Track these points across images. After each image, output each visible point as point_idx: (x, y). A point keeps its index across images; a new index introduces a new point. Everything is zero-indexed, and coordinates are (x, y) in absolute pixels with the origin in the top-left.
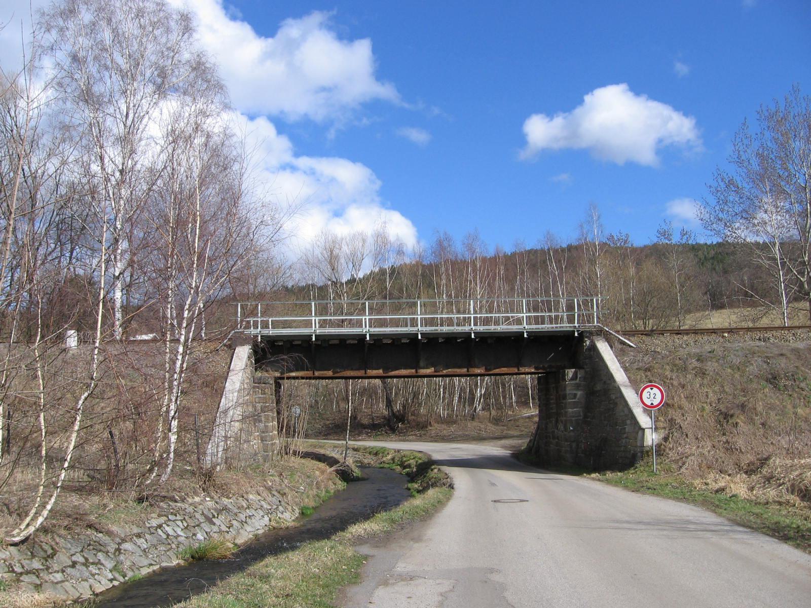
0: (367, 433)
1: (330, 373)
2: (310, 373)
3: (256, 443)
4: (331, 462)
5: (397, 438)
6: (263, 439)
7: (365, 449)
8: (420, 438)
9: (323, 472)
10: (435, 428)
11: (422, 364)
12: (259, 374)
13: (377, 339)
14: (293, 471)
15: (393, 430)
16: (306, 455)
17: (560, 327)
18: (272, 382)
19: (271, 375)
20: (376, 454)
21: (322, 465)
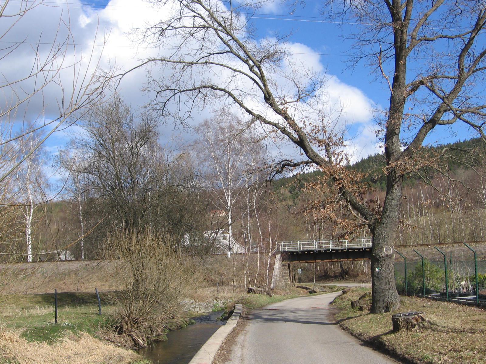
0: (332, 280)
1: (305, 261)
2: (299, 262)
3: (283, 283)
4: (307, 289)
5: (345, 282)
6: (285, 282)
7: (328, 286)
8: (354, 282)
9: (304, 292)
10: (359, 278)
11: (333, 258)
12: (283, 263)
13: (303, 252)
14: (294, 290)
15: (343, 278)
16: (298, 287)
17: (352, 245)
18: (287, 265)
19: (286, 263)
20: (332, 288)
21: (304, 290)
